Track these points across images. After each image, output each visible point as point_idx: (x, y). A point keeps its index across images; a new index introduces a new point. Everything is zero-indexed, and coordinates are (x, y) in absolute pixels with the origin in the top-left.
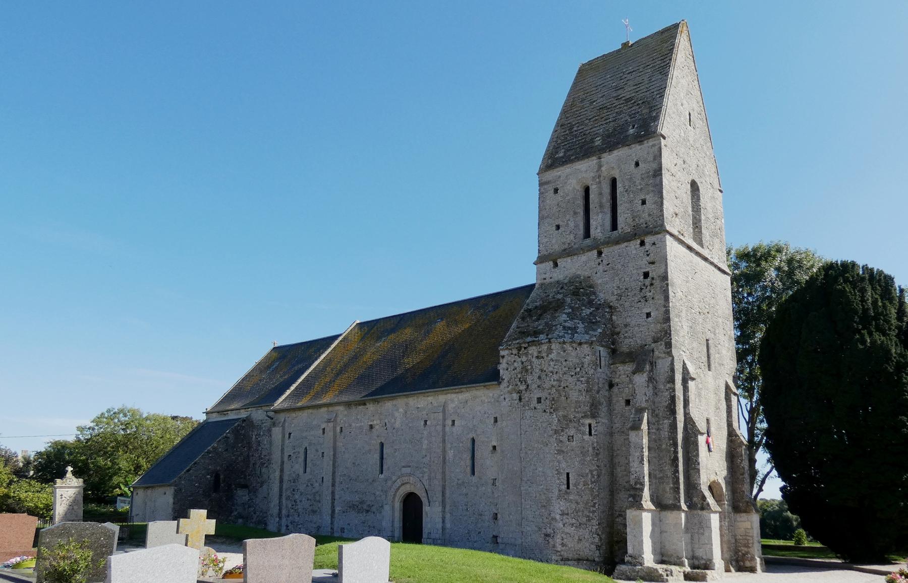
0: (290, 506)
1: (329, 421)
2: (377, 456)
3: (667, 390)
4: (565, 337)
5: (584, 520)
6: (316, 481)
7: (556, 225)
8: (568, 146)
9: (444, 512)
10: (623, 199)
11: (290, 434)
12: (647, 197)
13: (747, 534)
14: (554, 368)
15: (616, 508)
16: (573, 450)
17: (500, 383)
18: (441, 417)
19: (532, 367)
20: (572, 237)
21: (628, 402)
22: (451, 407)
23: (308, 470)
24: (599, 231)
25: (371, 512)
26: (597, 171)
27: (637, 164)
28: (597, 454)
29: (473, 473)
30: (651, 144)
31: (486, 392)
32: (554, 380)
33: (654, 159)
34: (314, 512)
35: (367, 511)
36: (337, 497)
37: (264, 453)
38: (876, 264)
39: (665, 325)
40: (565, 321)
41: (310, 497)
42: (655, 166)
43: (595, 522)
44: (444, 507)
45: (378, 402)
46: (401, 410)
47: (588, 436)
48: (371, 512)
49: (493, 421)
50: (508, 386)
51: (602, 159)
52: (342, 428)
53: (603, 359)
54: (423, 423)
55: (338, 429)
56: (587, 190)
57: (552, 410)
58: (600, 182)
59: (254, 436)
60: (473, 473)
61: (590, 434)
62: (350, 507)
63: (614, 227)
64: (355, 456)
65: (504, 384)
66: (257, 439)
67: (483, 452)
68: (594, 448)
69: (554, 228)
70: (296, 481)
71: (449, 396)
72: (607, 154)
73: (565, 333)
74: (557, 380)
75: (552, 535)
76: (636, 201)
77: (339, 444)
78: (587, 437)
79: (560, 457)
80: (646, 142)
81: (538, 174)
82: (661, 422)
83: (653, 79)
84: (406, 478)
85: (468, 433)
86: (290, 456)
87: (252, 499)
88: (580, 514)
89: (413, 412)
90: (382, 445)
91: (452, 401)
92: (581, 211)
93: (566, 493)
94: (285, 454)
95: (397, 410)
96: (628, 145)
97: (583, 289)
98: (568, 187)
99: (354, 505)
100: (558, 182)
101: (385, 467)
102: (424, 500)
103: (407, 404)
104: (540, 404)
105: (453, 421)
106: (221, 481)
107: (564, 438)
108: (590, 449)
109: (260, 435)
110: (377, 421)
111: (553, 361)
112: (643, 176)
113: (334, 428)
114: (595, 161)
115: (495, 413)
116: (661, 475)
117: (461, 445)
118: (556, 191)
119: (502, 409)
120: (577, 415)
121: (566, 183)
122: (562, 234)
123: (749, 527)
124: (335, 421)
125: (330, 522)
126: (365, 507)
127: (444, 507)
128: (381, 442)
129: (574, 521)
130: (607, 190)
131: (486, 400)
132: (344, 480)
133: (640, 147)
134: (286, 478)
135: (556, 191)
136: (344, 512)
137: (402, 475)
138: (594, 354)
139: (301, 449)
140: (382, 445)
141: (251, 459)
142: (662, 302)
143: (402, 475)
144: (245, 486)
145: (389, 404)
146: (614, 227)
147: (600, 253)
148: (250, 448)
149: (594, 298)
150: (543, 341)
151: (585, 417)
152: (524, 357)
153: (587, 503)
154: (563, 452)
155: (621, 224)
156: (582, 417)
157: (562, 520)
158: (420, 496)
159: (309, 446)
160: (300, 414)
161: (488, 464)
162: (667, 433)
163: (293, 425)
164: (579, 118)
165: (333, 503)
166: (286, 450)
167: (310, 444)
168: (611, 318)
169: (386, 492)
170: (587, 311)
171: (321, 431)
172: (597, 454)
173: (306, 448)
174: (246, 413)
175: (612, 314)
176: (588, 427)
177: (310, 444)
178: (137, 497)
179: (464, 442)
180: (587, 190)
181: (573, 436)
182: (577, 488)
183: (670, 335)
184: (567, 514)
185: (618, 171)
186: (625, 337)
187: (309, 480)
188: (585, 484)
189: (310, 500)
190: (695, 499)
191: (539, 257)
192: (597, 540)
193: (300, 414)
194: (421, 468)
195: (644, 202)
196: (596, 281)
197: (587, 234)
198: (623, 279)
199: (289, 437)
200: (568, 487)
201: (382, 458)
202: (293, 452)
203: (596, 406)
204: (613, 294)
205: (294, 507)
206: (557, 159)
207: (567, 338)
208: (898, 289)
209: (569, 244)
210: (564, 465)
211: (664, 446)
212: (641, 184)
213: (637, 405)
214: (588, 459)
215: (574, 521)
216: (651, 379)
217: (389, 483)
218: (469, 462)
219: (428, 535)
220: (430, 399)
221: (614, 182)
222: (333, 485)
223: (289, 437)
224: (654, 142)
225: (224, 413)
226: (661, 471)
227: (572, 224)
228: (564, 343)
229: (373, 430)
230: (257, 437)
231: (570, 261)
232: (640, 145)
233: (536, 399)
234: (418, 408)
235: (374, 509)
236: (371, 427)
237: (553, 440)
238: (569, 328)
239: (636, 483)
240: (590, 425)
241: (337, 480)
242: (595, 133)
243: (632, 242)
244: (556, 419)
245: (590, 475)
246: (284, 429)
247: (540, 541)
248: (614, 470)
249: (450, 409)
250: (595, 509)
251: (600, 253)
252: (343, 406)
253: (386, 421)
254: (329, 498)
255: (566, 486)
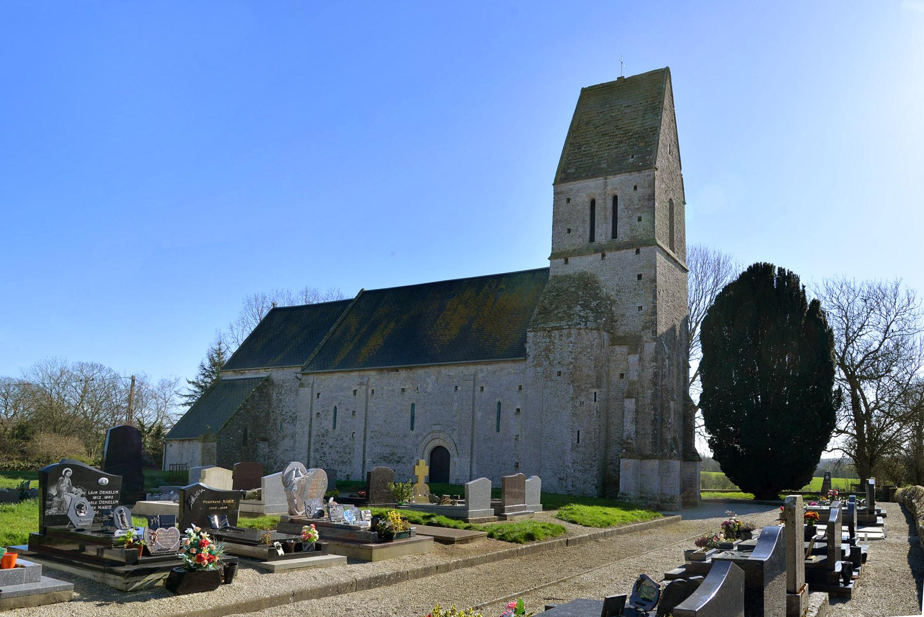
0: (318, 457)
1: (361, 384)
2: (408, 416)
3: (651, 367)
4: (581, 325)
5: (588, 467)
6: (346, 436)
7: (568, 229)
8: (578, 163)
9: (471, 462)
10: (624, 215)
11: (319, 394)
12: (643, 216)
13: (692, 477)
14: (572, 349)
15: (608, 458)
16: (583, 413)
17: (525, 360)
18: (472, 384)
19: (554, 348)
20: (581, 240)
21: (622, 376)
22: (480, 375)
23: (338, 426)
24: (603, 238)
25: (402, 463)
26: (604, 189)
27: (635, 188)
28: (599, 416)
29: (498, 430)
30: (647, 173)
31: (512, 364)
32: (572, 358)
33: (649, 186)
34: (344, 463)
35: (398, 462)
36: (367, 450)
37: (285, 410)
38: (788, 267)
39: (652, 317)
40: (580, 311)
41: (339, 450)
42: (650, 192)
43: (595, 469)
44: (472, 458)
45: (411, 370)
46: (433, 377)
47: (593, 402)
48: (402, 463)
49: (518, 388)
50: (533, 362)
51: (608, 180)
52: (373, 390)
53: (605, 341)
54: (454, 388)
55: (370, 391)
56: (593, 203)
57: (569, 382)
58: (605, 199)
59: (275, 395)
60: (498, 430)
61: (595, 401)
62: (381, 458)
63: (615, 235)
64: (387, 415)
65: (530, 360)
66: (278, 397)
67: (508, 414)
68: (597, 412)
69: (566, 231)
70: (325, 436)
71: (479, 367)
72: (612, 176)
73: (581, 321)
74: (574, 358)
75: (565, 479)
76: (634, 217)
77: (371, 404)
78: (592, 403)
79: (574, 419)
80: (643, 171)
81: (553, 185)
82: (645, 392)
83: (647, 117)
84: (437, 434)
85: (495, 398)
86: (319, 413)
87: (272, 451)
88: (585, 462)
89: (445, 379)
90: (413, 405)
91: (482, 371)
92: (588, 219)
93: (577, 446)
94: (313, 411)
95: (430, 377)
96: (629, 172)
97: (590, 284)
98: (579, 199)
99: (384, 457)
100: (571, 194)
101: (416, 425)
102: (452, 452)
103: (439, 372)
104: (560, 377)
105: (482, 388)
106: (248, 436)
107: (578, 404)
108: (595, 412)
109: (281, 393)
110: (409, 385)
111: (572, 343)
112: (640, 198)
113: (367, 390)
114: (602, 181)
115: (520, 382)
116: (643, 432)
117: (489, 407)
118: (569, 200)
119: (527, 379)
120: (587, 386)
121: (577, 195)
122: (572, 237)
123: (694, 472)
124: (367, 384)
125: (361, 471)
126: (396, 458)
127: (472, 458)
128: (413, 404)
129: (582, 468)
130: (610, 204)
131: (513, 372)
132: (375, 435)
133: (638, 175)
134: (314, 433)
135: (569, 200)
136: (374, 463)
137: (433, 432)
138: (600, 338)
139: (331, 407)
140: (413, 405)
141: (271, 415)
142: (651, 299)
143: (433, 432)
144: (265, 440)
145: (421, 371)
146: (615, 235)
147: (603, 255)
148: (270, 405)
149: (599, 292)
150: (564, 327)
151: (593, 387)
152: (548, 339)
153: (591, 454)
154: (576, 414)
155: (621, 234)
156: (590, 387)
157: (573, 467)
158: (447, 448)
159: (339, 405)
160: (330, 377)
161: (513, 425)
162: (649, 400)
163: (322, 386)
164: (585, 140)
165: (364, 455)
166: (314, 408)
167: (340, 404)
168: (611, 309)
169: (417, 445)
170: (594, 304)
171: (352, 393)
172: (599, 416)
173: (336, 407)
174: (266, 373)
175: (611, 305)
176: (594, 395)
177: (340, 404)
178: (170, 449)
179: (492, 405)
180: (593, 203)
181: (583, 402)
182: (585, 443)
183: (656, 325)
184: (577, 463)
185: (620, 191)
186: (621, 325)
187: (339, 435)
188: (590, 439)
189: (340, 452)
190: (665, 450)
191: (552, 254)
192: (596, 482)
193: (330, 377)
194: (450, 426)
195: (640, 219)
196: (600, 278)
197: (592, 239)
198: (621, 279)
199: (318, 397)
200: (578, 442)
201: (413, 418)
202: (321, 410)
203: (600, 379)
204: (613, 289)
205: (322, 458)
206: (569, 174)
207: (582, 326)
208: (787, 272)
209: (578, 245)
210: (576, 425)
211: (647, 410)
212: (638, 205)
213: (630, 378)
214: (593, 419)
215: (582, 468)
216: (641, 359)
217: (420, 438)
218: (495, 422)
219: (456, 481)
220: (461, 368)
221: (615, 198)
222: (365, 440)
223: (318, 397)
224: (650, 173)
225: (241, 372)
226: (644, 429)
227: (581, 230)
228: (580, 329)
229: (405, 393)
230: (278, 395)
231: (579, 260)
232: (638, 173)
233: (556, 373)
234: (450, 376)
235: (404, 460)
236: (403, 390)
237: (569, 405)
238: (583, 317)
239: (627, 439)
240: (595, 393)
241: (368, 435)
242: (600, 156)
243: (630, 250)
244: (573, 389)
245: (593, 432)
246: (312, 390)
247: (555, 484)
248: (609, 428)
249: (479, 377)
250: (596, 458)
251: (603, 255)
252: (375, 372)
253: (418, 385)
254: (361, 451)
255: (577, 441)
